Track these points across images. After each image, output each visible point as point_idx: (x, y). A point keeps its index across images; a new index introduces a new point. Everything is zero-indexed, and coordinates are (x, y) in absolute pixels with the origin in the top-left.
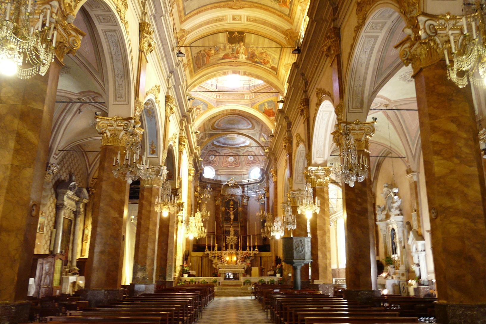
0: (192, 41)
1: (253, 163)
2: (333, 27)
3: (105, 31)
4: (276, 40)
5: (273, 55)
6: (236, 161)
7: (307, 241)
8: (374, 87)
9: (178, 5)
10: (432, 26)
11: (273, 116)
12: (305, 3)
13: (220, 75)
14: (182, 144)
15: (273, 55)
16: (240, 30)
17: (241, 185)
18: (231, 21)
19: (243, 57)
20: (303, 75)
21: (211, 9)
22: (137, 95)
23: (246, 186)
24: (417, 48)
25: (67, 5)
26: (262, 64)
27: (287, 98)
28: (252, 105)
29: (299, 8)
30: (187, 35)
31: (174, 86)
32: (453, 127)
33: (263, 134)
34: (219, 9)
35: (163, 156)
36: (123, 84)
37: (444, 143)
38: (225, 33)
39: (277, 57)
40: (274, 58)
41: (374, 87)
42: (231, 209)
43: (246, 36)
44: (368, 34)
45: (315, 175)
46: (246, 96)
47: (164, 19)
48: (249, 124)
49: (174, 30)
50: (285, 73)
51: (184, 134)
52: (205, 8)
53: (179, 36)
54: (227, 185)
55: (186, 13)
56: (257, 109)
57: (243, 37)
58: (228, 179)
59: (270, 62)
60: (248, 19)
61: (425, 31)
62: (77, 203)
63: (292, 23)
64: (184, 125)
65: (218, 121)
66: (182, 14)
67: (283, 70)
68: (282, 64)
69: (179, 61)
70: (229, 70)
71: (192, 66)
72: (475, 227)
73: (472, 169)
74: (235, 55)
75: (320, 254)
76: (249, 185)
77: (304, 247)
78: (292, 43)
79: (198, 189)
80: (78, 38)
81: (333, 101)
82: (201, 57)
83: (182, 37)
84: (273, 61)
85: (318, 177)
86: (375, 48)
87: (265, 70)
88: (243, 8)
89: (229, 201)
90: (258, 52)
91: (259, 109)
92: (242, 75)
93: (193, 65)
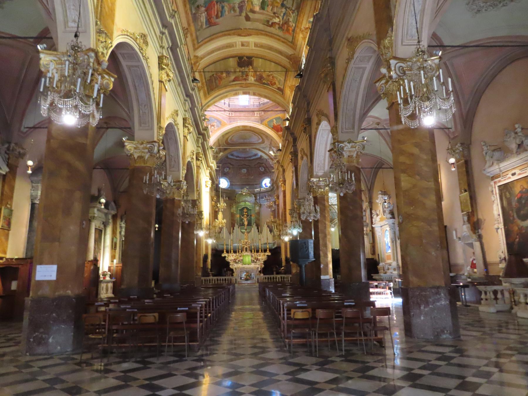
0: (205, 66)
2: (329, 57)
3: (129, 67)
7: (311, 243)
8: (364, 110)
9: (191, 35)
10: (401, 68)
11: (281, 131)
12: (306, 31)
13: (232, 96)
14: (199, 160)
15: (279, 77)
16: (248, 55)
17: (253, 194)
18: (241, 47)
19: (252, 79)
20: (305, 96)
21: (221, 36)
22: (159, 121)
24: (390, 85)
25: (101, 54)
27: (292, 116)
28: (262, 121)
31: (191, 109)
32: (416, 151)
35: (183, 173)
36: (147, 112)
37: (409, 163)
38: (235, 58)
39: (282, 79)
40: (280, 80)
41: (364, 110)
44: (357, 66)
45: (316, 186)
47: (180, 51)
49: (189, 59)
50: (290, 94)
51: (200, 150)
53: (193, 62)
56: (266, 125)
59: (277, 83)
60: (256, 45)
61: (396, 73)
62: (106, 214)
63: (295, 49)
64: (200, 141)
65: (231, 136)
66: (196, 42)
70: (240, 91)
71: (206, 89)
72: (431, 229)
73: (430, 183)
75: (321, 253)
76: (261, 194)
77: (308, 248)
79: (215, 198)
80: (110, 80)
81: (329, 121)
83: (195, 63)
84: (279, 83)
85: (320, 187)
86: (364, 77)
89: (243, 209)
91: (268, 126)
92: (251, 95)
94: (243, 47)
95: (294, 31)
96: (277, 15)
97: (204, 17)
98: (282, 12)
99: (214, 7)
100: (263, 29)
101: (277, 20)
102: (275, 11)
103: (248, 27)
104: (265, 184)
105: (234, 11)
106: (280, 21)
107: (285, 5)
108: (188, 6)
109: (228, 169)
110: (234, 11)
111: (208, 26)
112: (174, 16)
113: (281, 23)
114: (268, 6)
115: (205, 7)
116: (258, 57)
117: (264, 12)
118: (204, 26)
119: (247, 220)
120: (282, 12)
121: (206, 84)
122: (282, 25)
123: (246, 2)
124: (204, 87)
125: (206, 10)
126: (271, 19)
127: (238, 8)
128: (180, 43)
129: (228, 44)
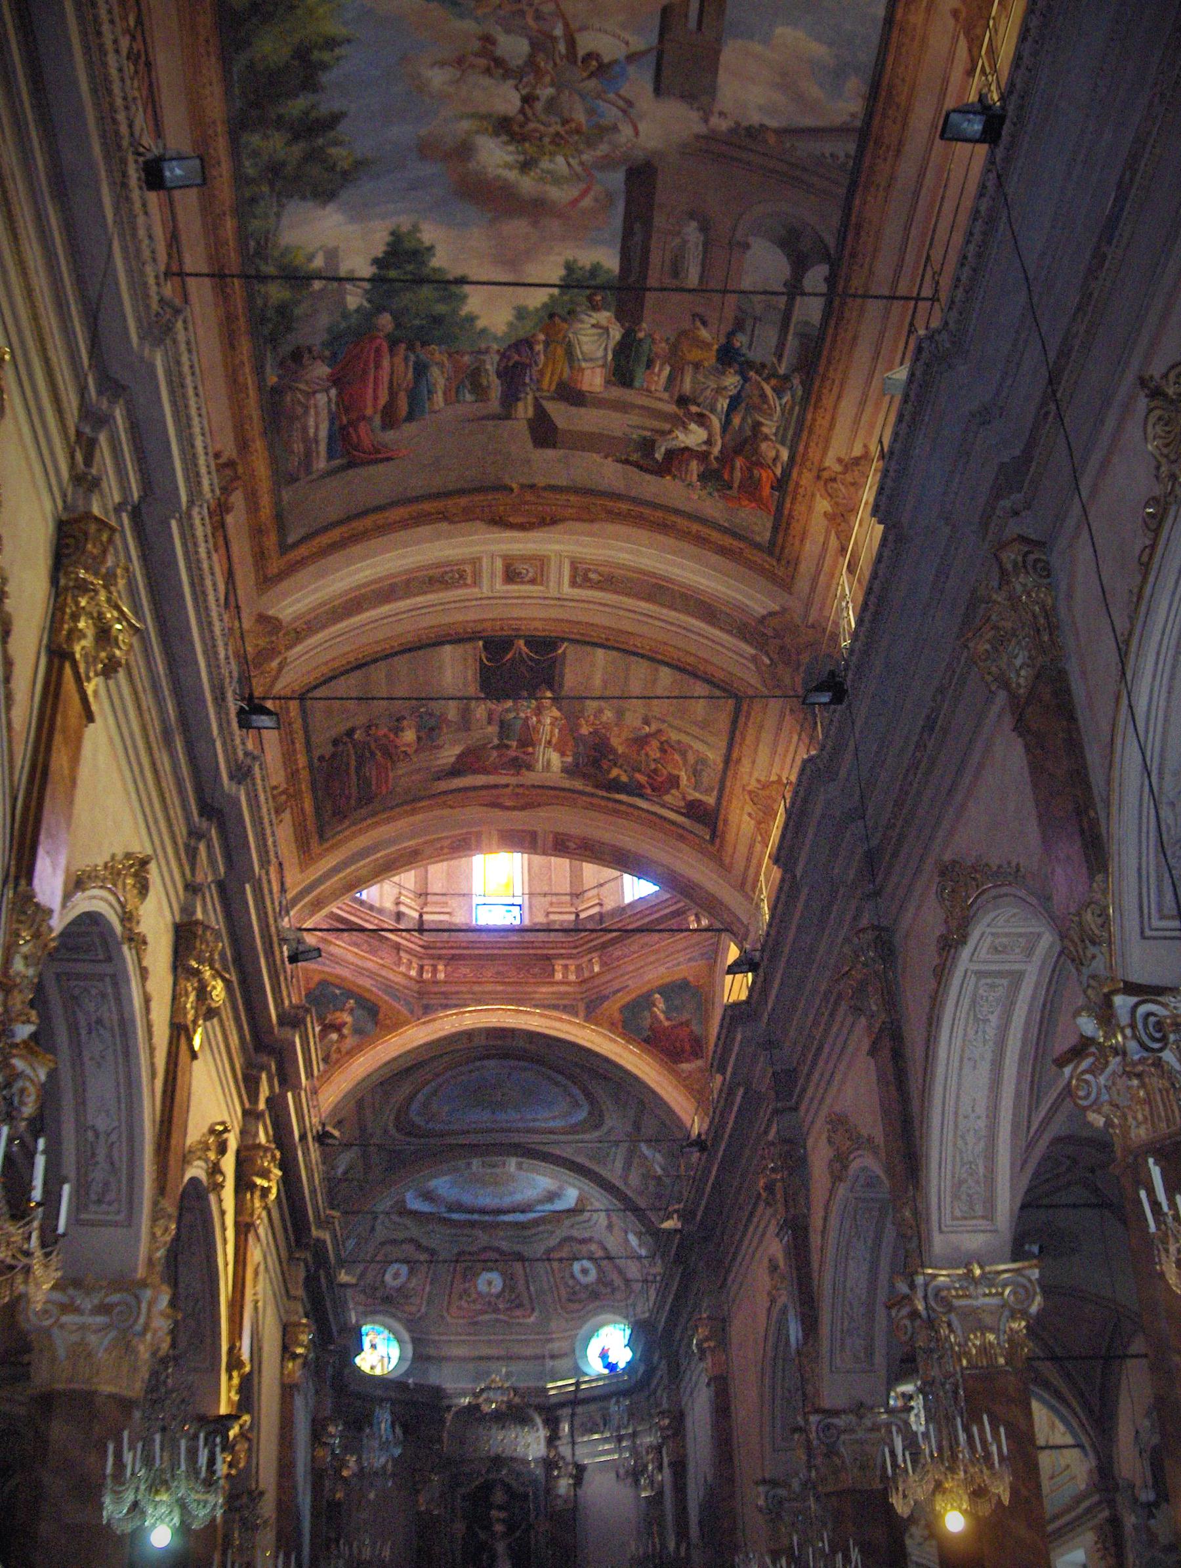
0: (311, 679)
1: (595, 1295)
4: (710, 669)
5: (698, 746)
6: (512, 1289)
9: (253, 506)
14: (252, 1187)
15: (698, 746)
16: (538, 628)
17: (539, 1408)
18: (500, 587)
23: (566, 1411)
26: (641, 796)
29: (823, 505)
30: (289, 647)
33: (644, 1148)
34: (444, 526)
39: (714, 756)
40: (703, 761)
42: (499, 1528)
43: (570, 656)
46: (558, 965)
48: (576, 1105)
52: (379, 518)
54: (473, 1409)
55: (290, 540)
56: (612, 1026)
57: (554, 661)
58: (478, 1377)
59: (684, 781)
60: (581, 576)
64: (264, 1092)
66: (271, 540)
67: (746, 818)
68: (738, 790)
69: (246, 754)
71: (308, 804)
74: (512, 753)
78: (788, 681)
82: (353, 763)
84: (696, 773)
87: (656, 822)
88: (554, 521)
89: (487, 1488)
90: (624, 735)
93: (315, 798)
94: (513, 587)
95: (781, 484)
96: (694, 409)
97: (324, 414)
98: (720, 390)
99: (378, 366)
100: (619, 485)
101: (693, 437)
102: (687, 387)
103: (541, 481)
104: (604, 1355)
105: (480, 391)
106: (709, 442)
107: (737, 352)
108: (245, 345)
109: (404, 1269)
110: (480, 391)
111: (337, 462)
112: (169, 329)
113: (716, 450)
114: (650, 364)
115: (332, 360)
116: (588, 641)
117: (628, 395)
118: (321, 464)
119: (509, 1546)
120: (720, 390)
121: (313, 783)
122: (725, 458)
123: (539, 347)
124: (297, 796)
125: (336, 381)
126: (663, 433)
127: (499, 375)
128: (190, 494)
129: (438, 566)
